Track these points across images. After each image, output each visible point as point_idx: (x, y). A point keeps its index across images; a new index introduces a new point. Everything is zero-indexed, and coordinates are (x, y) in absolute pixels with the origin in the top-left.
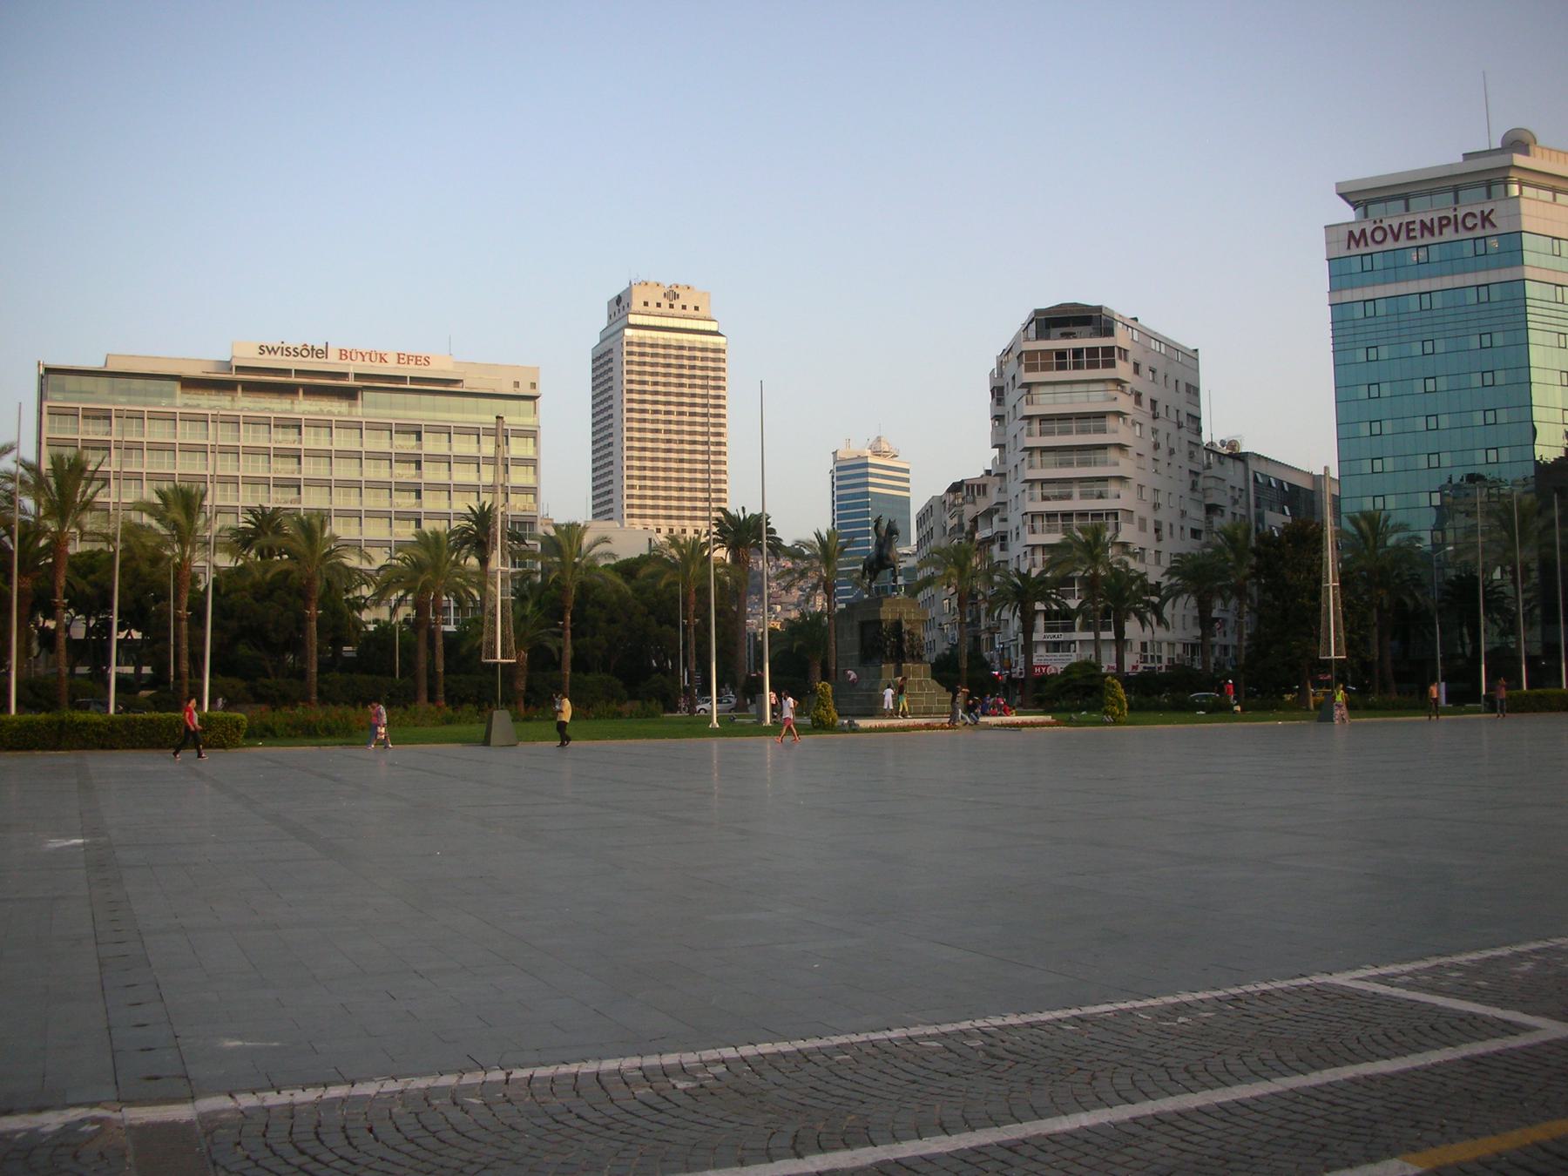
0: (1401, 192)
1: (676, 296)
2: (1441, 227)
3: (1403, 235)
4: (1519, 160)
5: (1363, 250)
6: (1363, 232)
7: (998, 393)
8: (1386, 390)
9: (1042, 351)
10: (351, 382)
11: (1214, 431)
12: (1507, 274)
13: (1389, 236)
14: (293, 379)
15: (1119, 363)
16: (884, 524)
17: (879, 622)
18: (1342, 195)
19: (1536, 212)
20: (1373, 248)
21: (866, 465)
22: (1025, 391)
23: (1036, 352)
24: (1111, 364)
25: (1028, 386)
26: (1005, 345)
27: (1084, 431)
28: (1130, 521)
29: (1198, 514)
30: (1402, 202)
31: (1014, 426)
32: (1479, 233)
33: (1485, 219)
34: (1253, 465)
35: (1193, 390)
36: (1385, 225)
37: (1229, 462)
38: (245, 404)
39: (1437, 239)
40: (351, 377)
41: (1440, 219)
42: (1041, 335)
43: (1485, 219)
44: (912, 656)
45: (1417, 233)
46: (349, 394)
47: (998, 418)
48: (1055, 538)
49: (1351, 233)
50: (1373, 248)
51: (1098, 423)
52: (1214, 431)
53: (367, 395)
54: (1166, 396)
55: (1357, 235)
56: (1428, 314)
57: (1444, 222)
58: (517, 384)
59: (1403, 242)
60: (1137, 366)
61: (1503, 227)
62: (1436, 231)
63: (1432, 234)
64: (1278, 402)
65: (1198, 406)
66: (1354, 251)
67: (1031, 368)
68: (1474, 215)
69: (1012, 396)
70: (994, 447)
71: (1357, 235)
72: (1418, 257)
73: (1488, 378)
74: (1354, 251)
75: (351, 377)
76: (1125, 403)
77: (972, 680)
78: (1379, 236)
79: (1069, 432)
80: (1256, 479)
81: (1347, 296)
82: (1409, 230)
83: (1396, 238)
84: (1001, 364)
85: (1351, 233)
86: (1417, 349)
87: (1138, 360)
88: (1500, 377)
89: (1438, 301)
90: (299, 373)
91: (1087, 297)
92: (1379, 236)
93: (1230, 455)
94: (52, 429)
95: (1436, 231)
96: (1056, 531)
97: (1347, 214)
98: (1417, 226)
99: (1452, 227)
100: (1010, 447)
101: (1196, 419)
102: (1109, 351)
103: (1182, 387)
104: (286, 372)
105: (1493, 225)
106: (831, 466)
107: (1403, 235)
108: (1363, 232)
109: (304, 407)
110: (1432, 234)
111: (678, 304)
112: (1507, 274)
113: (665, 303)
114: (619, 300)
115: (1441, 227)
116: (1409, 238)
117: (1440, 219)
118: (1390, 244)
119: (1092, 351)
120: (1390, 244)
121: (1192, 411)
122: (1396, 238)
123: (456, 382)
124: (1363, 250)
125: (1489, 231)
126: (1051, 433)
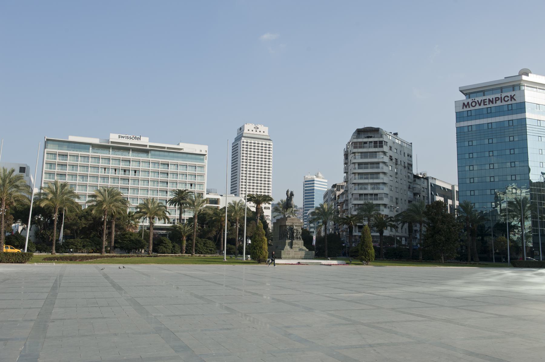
0: (482, 90)
1: (258, 128)
2: (496, 101)
3: (482, 104)
4: (524, 78)
5: (468, 109)
6: (468, 103)
7: (346, 156)
8: (475, 155)
9: (359, 142)
10: (148, 148)
11: (416, 171)
12: (519, 116)
13: (478, 104)
14: (129, 146)
15: (384, 146)
16: (290, 193)
17: (286, 226)
18: (461, 91)
19: (530, 96)
20: (471, 108)
21: (314, 180)
22: (353, 155)
23: (357, 142)
24: (382, 147)
25: (354, 153)
26: (349, 141)
27: (372, 168)
28: (387, 197)
29: (410, 194)
30: (482, 93)
31: (351, 166)
32: (509, 102)
33: (512, 98)
34: (430, 181)
35: (410, 156)
36: (476, 101)
37: (422, 180)
38: (111, 154)
39: (494, 105)
40: (148, 146)
41: (496, 98)
42: (358, 137)
43: (512, 98)
44: (297, 238)
45: (487, 103)
46: (146, 152)
47: (346, 163)
48: (362, 202)
49: (464, 104)
50: (471, 108)
51: (377, 165)
52: (416, 171)
53: (152, 152)
54: (401, 158)
55: (466, 104)
56: (491, 130)
57: (497, 99)
58: (201, 151)
59: (482, 106)
60: (391, 147)
61: (518, 101)
62: (494, 102)
63: (493, 103)
64: (440, 165)
65: (412, 161)
66: (465, 109)
67: (355, 148)
68: (508, 97)
69: (350, 157)
70: (345, 173)
71: (466, 104)
72: (488, 120)
73: (512, 151)
74: (465, 109)
75: (148, 146)
76: (386, 159)
77: (326, 247)
78: (474, 104)
79: (367, 168)
80: (431, 185)
81: (462, 124)
82: (484, 102)
83: (480, 105)
84: (347, 146)
85: (464, 104)
86: (486, 141)
87: (391, 146)
88: (517, 151)
89: (494, 126)
90: (131, 144)
91: (374, 125)
92: (474, 104)
93: (423, 177)
94: (47, 158)
95: (494, 102)
96: (362, 200)
97: (463, 97)
98: (487, 101)
99: (500, 101)
100: (349, 173)
101: (411, 165)
102: (381, 142)
103: (406, 155)
104: (127, 144)
105: (515, 100)
106: (304, 181)
107: (482, 104)
108: (468, 103)
109: (131, 156)
110: (493, 103)
111: (258, 130)
112: (519, 116)
113: (254, 130)
114: (241, 129)
115: (496, 101)
116: (484, 105)
117: (496, 98)
118: (477, 107)
119: (375, 142)
120: (477, 107)
121: (410, 162)
122: (480, 105)
123: (181, 149)
124: (468, 109)
125: (513, 102)
126: (362, 168)
